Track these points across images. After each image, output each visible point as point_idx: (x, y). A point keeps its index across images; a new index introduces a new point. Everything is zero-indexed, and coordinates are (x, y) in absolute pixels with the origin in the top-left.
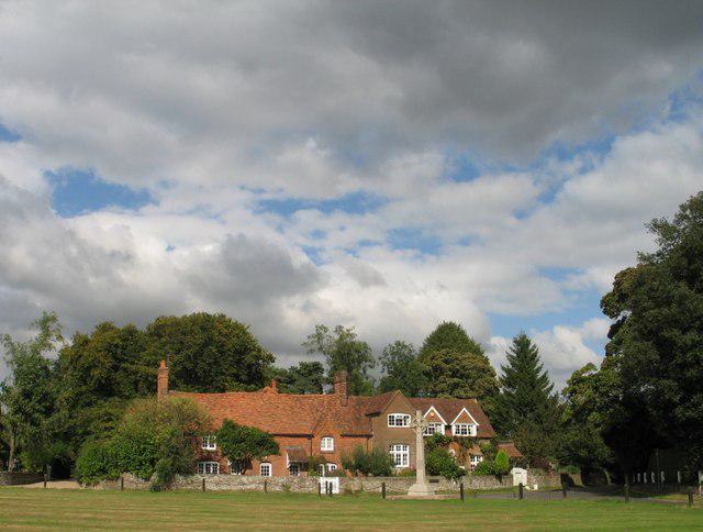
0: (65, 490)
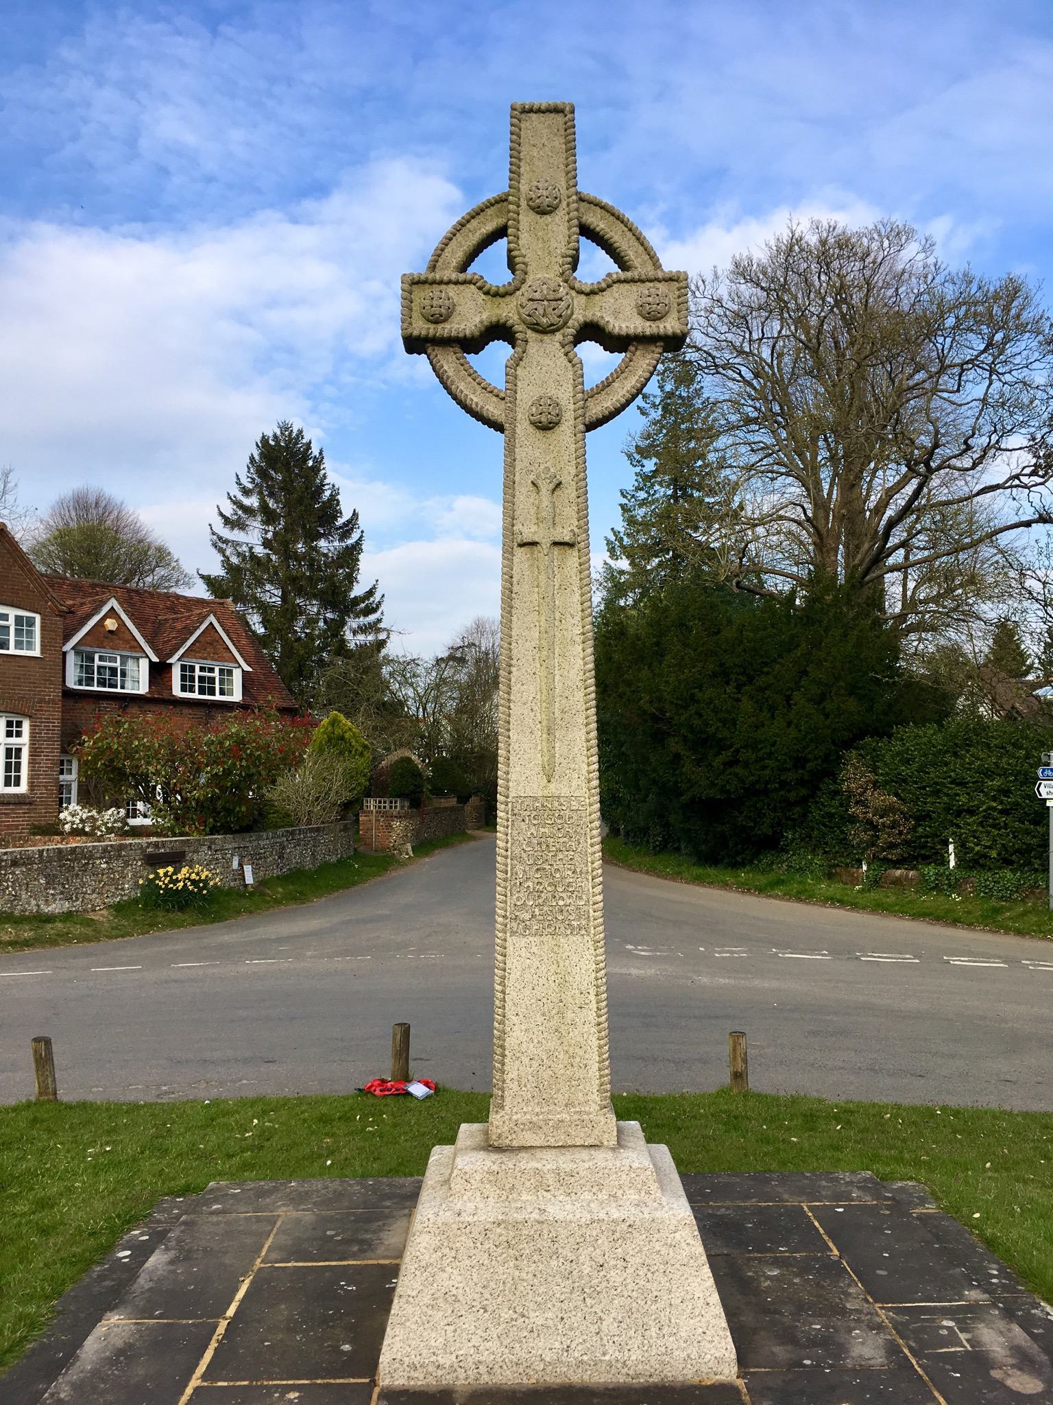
0: (32, 763)
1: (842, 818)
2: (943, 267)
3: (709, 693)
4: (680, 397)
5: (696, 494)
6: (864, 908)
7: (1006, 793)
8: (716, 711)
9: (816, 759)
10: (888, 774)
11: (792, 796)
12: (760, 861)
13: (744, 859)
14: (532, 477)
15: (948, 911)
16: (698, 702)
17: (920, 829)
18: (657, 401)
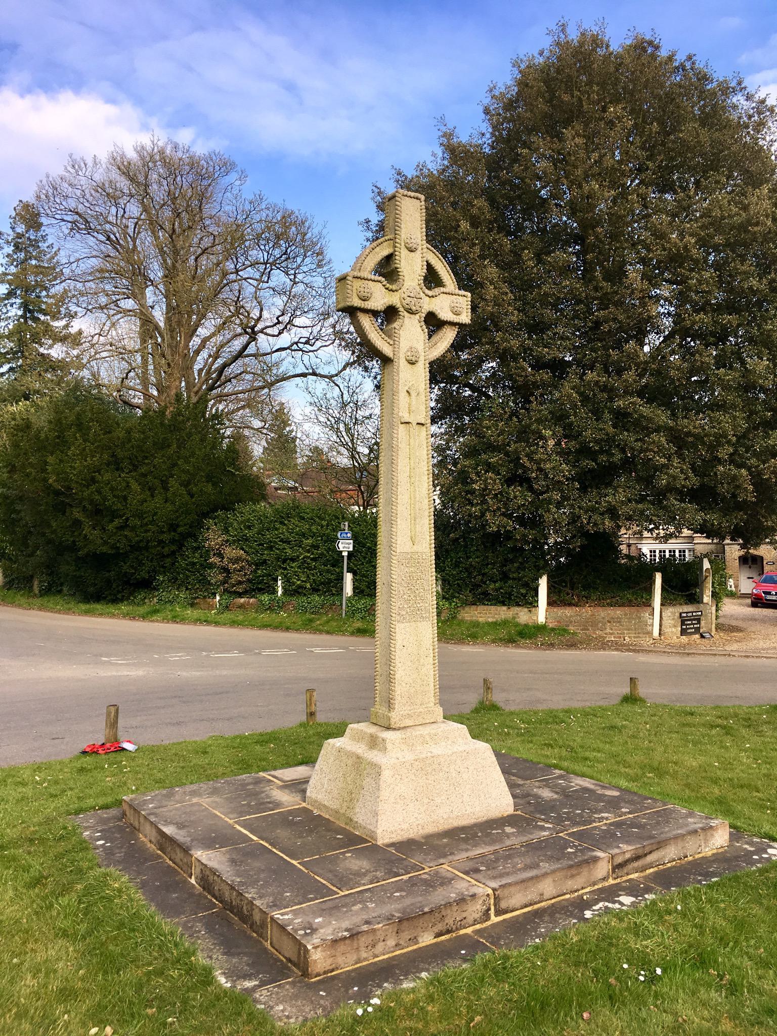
1: (201, 565)
2: (265, 198)
3: (107, 476)
4: (29, 238)
5: (42, 318)
6: (225, 625)
7: (316, 547)
8: (112, 489)
9: (185, 525)
10: (236, 536)
11: (166, 551)
12: (135, 598)
13: (123, 596)
14: (407, 388)
15: (281, 623)
16: (98, 482)
17: (259, 572)
18: (10, 239)
